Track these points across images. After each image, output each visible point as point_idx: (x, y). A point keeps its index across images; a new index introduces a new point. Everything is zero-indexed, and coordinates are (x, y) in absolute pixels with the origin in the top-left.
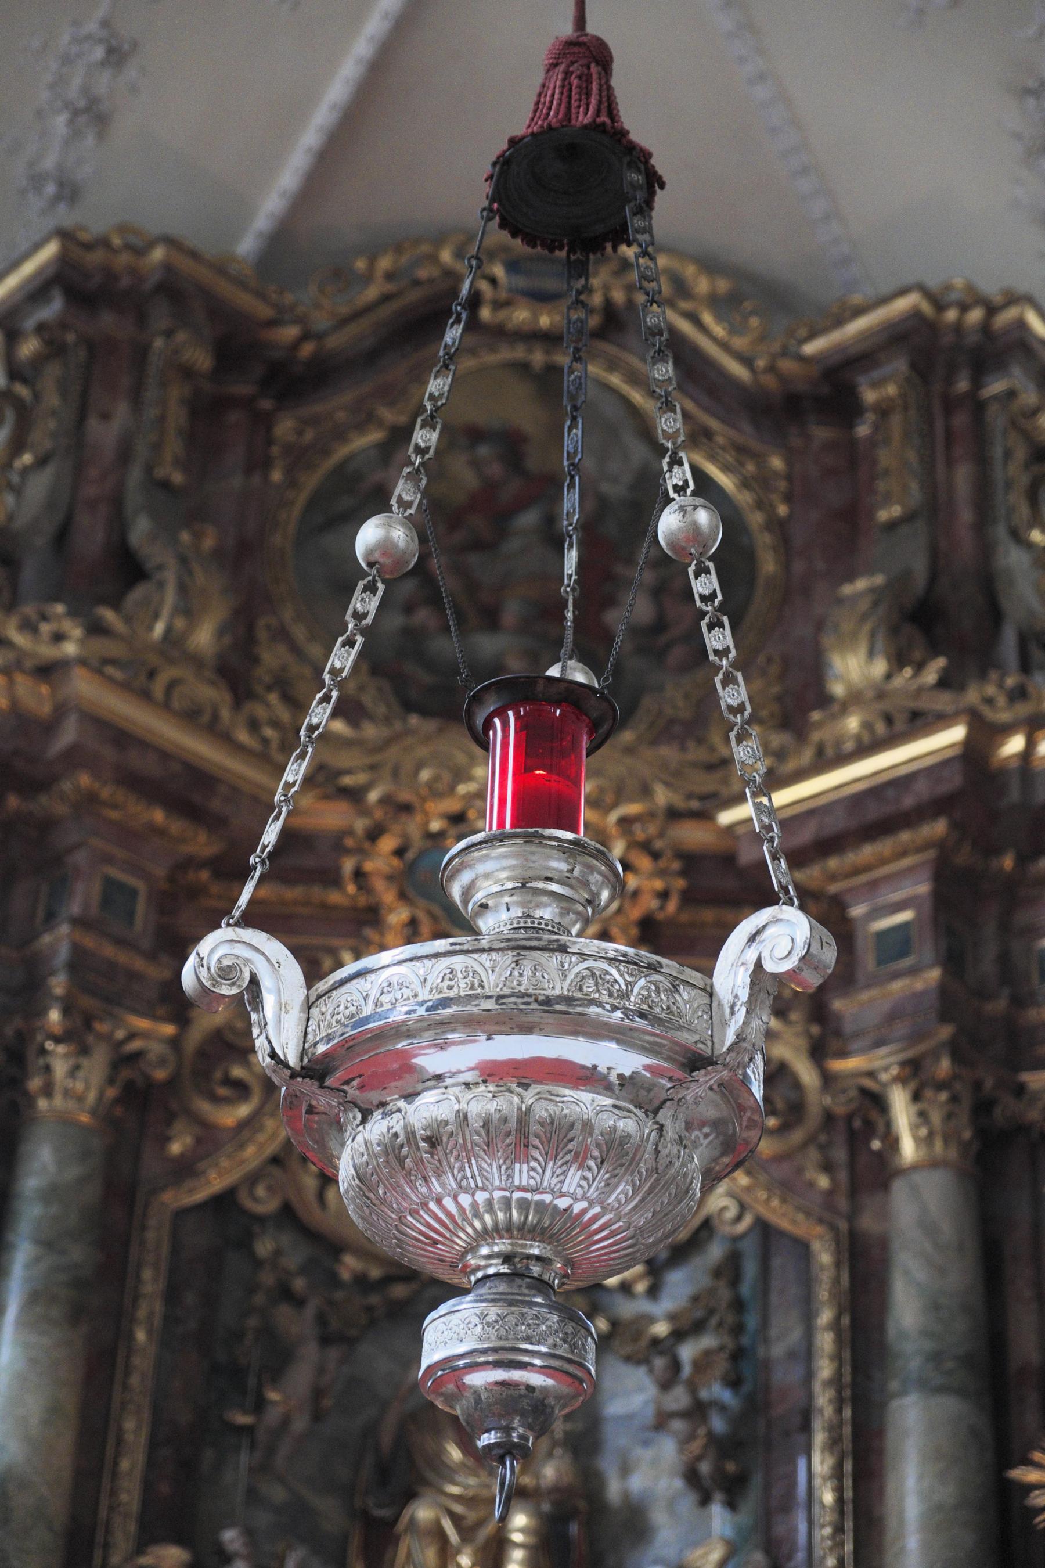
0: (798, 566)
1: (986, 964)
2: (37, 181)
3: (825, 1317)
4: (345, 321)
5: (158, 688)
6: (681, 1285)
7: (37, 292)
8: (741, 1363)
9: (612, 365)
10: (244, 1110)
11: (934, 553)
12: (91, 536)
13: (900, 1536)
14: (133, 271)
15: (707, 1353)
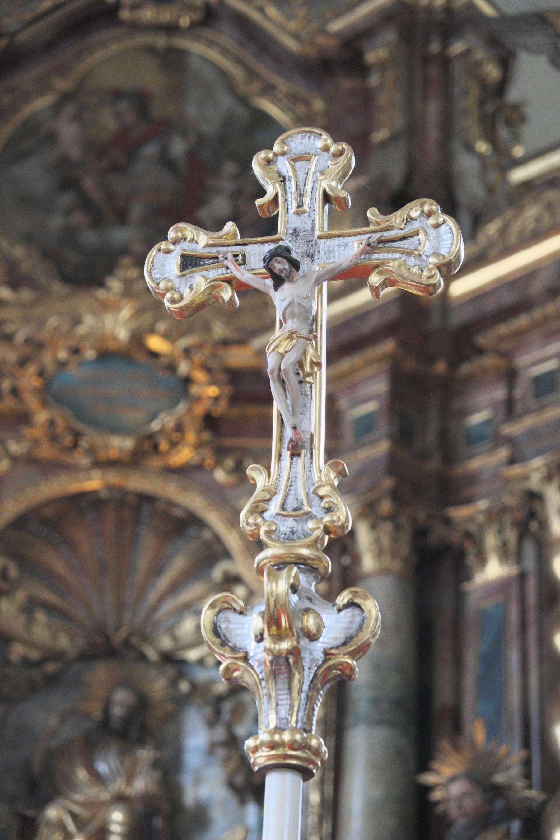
9: (211, 44)
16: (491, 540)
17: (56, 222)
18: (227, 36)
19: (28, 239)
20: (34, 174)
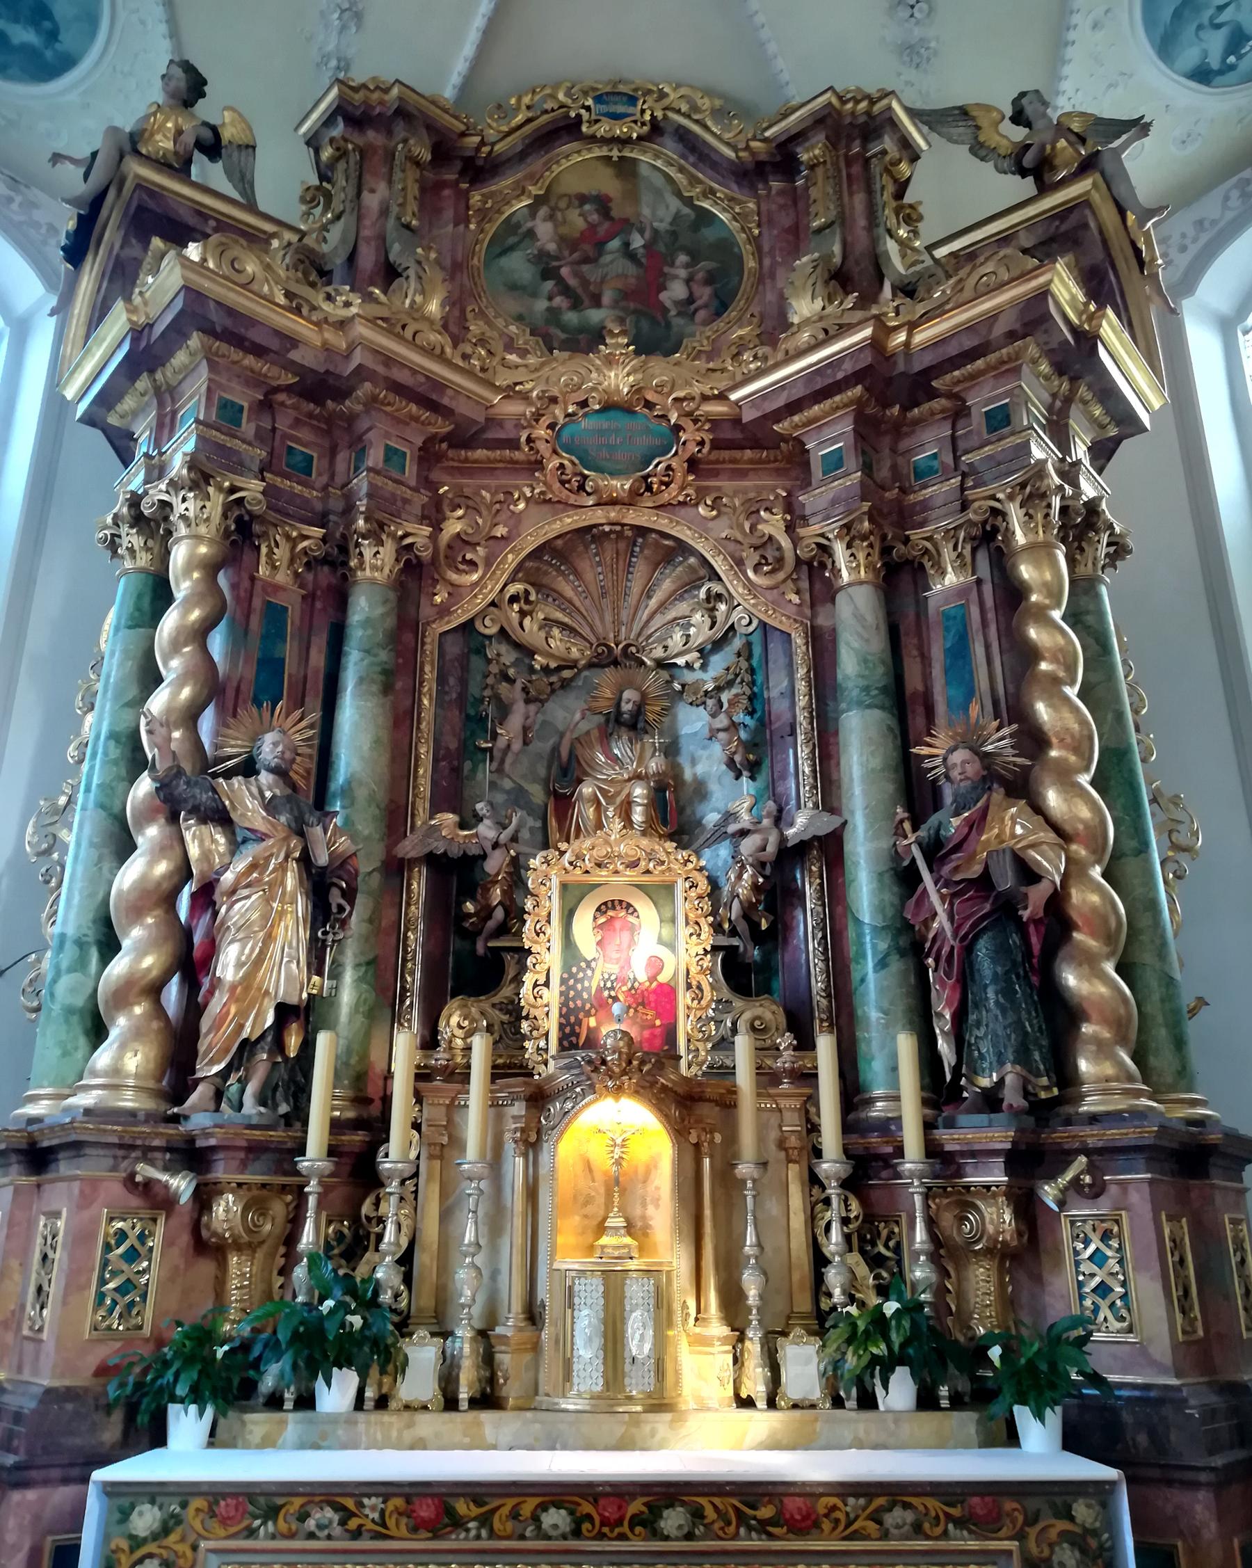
0: (767, 262)
1: (884, 473)
2: (326, 58)
3: (801, 672)
4: (508, 134)
5: (408, 334)
6: (719, 663)
7: (329, 121)
8: (755, 703)
9: (657, 156)
10: (475, 577)
11: (845, 244)
12: (368, 259)
13: (851, 788)
14: (382, 103)
15: (736, 695)
16: (947, 554)
17: (541, 305)
18: (670, 148)
19: (520, 318)
20: (518, 265)
